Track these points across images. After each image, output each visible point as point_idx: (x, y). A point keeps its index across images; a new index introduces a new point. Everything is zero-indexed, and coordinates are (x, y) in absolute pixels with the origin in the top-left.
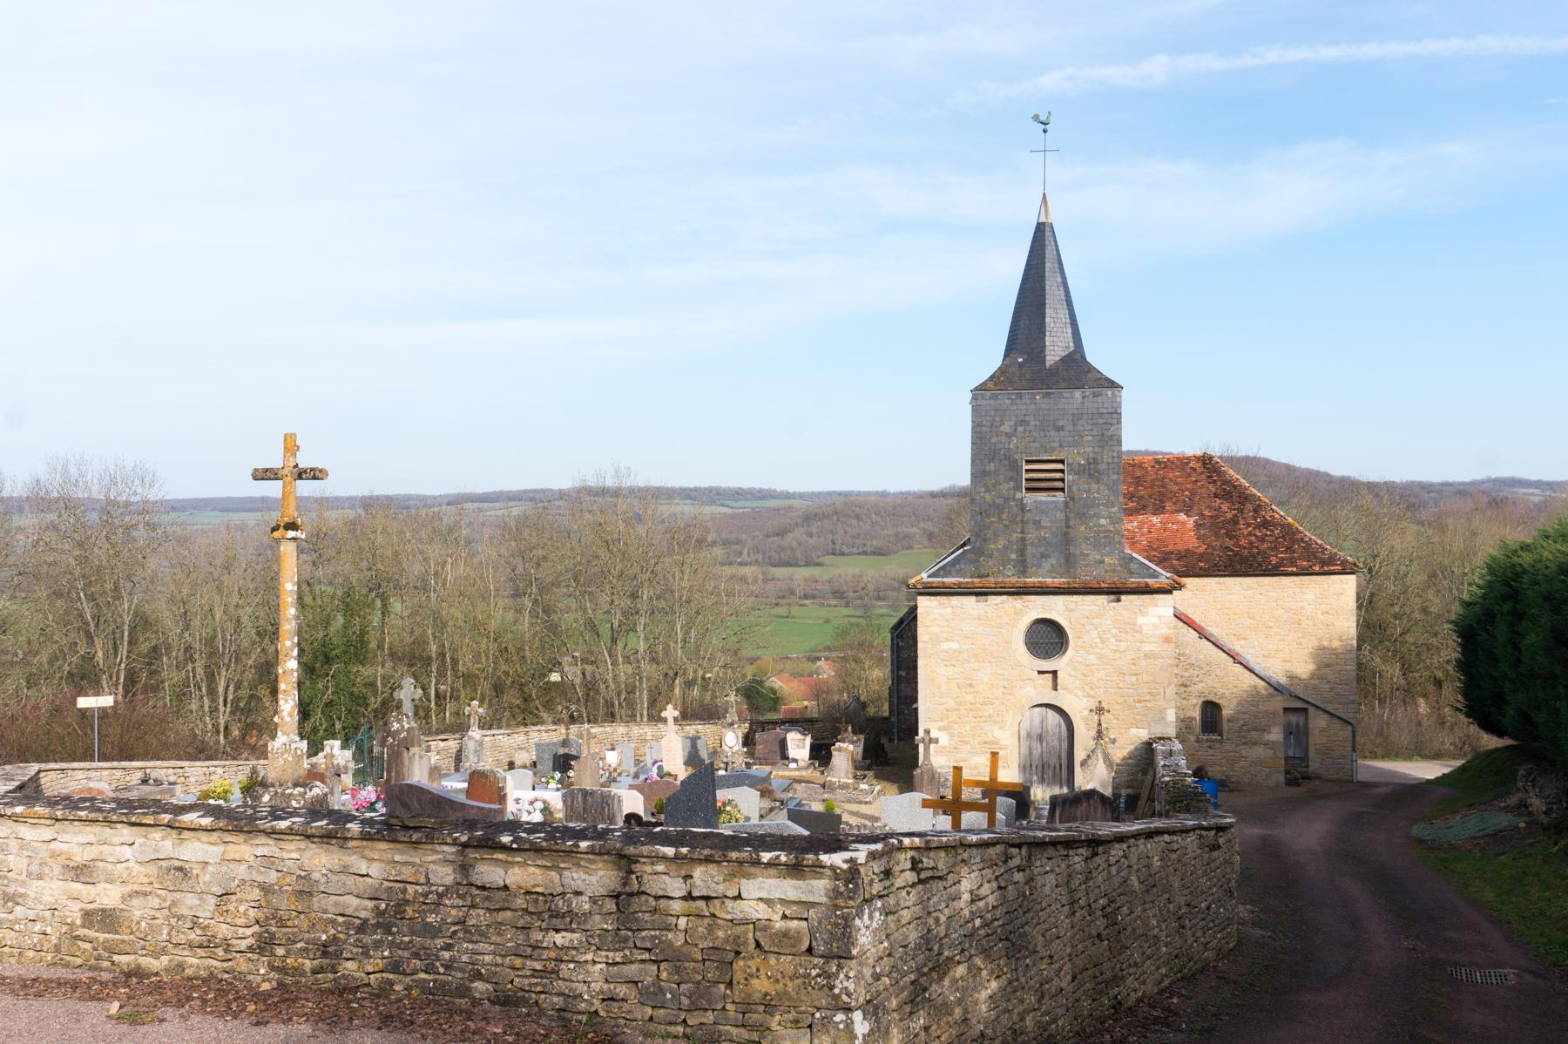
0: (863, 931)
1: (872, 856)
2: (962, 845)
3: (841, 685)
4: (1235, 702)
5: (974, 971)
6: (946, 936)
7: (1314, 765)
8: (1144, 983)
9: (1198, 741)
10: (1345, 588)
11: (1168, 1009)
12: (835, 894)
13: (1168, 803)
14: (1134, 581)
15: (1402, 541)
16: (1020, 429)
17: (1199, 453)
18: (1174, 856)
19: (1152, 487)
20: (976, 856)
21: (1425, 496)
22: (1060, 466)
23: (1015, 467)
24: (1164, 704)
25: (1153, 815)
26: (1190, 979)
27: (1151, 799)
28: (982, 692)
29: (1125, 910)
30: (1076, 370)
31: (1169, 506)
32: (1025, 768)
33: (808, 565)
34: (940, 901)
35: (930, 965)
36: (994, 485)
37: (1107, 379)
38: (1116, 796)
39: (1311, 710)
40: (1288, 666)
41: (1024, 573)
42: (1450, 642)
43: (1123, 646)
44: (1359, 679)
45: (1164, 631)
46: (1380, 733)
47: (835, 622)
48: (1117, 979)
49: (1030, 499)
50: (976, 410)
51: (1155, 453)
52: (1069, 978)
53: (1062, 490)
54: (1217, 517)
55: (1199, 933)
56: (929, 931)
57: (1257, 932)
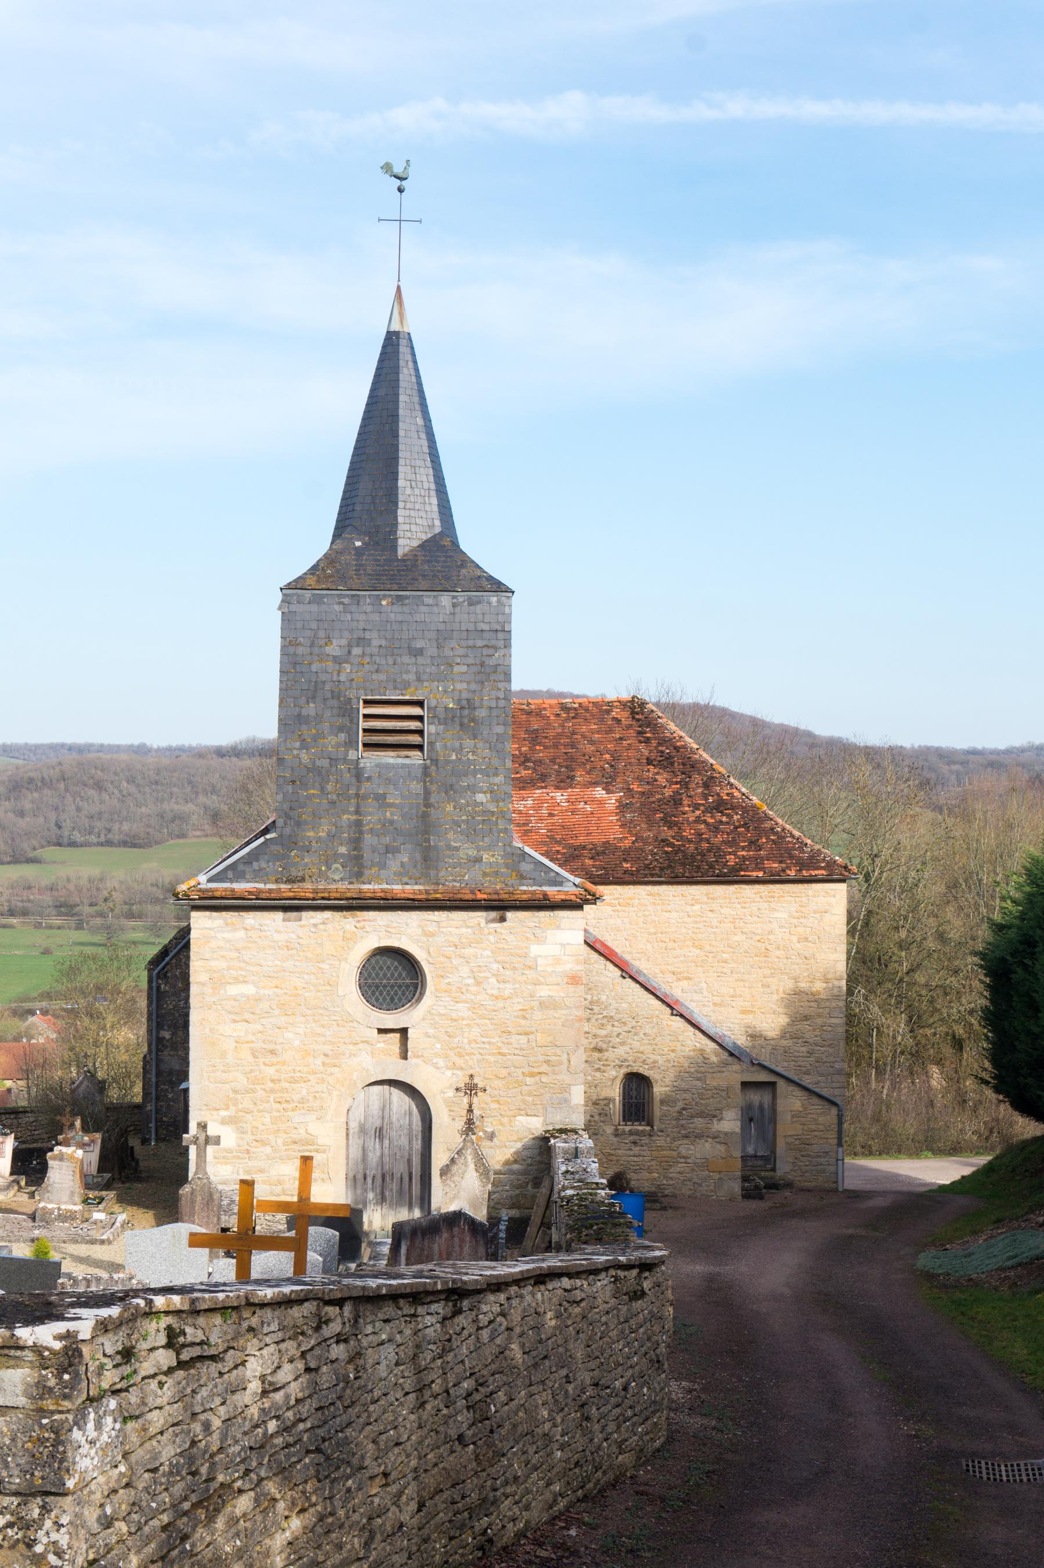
0: (85, 1449)
1: (103, 1327)
2: (249, 1304)
3: (67, 1054)
4: (671, 1075)
5: (265, 1504)
6: (221, 1450)
7: (784, 1168)
8: (527, 1508)
9: (616, 1134)
10: (829, 905)
11: (562, 1546)
12: (42, 1390)
13: (571, 1229)
14: (526, 889)
15: (913, 833)
16: (356, 651)
17: (625, 696)
18: (577, 1310)
19: (556, 746)
20: (272, 1321)
21: (945, 769)
22: (416, 711)
23: (347, 711)
24: (567, 1079)
25: (548, 1249)
26: (595, 1498)
27: (546, 1224)
28: (299, 1067)
29: (501, 1396)
30: (443, 563)
31: (580, 776)
32: (356, 1180)
33: (15, 861)
34: (212, 1395)
35: (194, 1498)
36: (315, 739)
37: (490, 578)
38: (494, 1220)
39: (781, 1084)
40: (749, 1019)
41: (358, 876)
42: (976, 983)
43: (508, 989)
44: (850, 1038)
45: (570, 966)
46: (876, 1118)
47: (58, 954)
48: (487, 1505)
49: (371, 760)
50: (288, 619)
51: (562, 695)
52: (413, 1506)
53: (420, 747)
54: (650, 794)
55: (611, 1427)
56: (193, 1443)
57: (695, 1422)
